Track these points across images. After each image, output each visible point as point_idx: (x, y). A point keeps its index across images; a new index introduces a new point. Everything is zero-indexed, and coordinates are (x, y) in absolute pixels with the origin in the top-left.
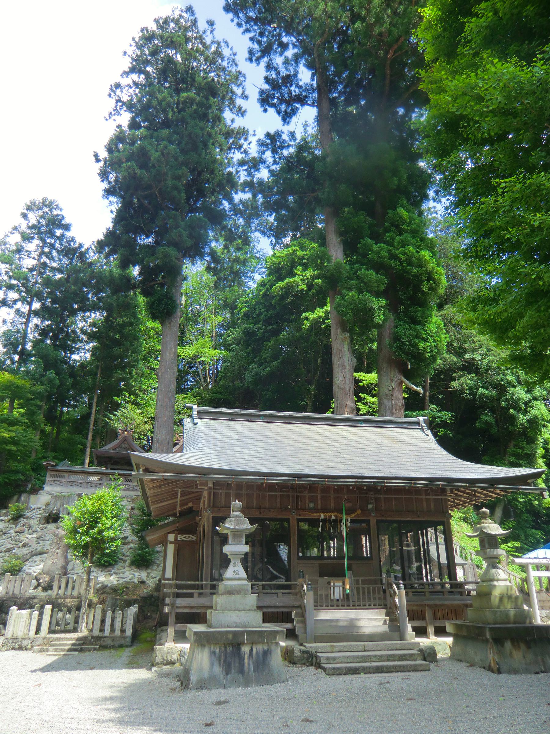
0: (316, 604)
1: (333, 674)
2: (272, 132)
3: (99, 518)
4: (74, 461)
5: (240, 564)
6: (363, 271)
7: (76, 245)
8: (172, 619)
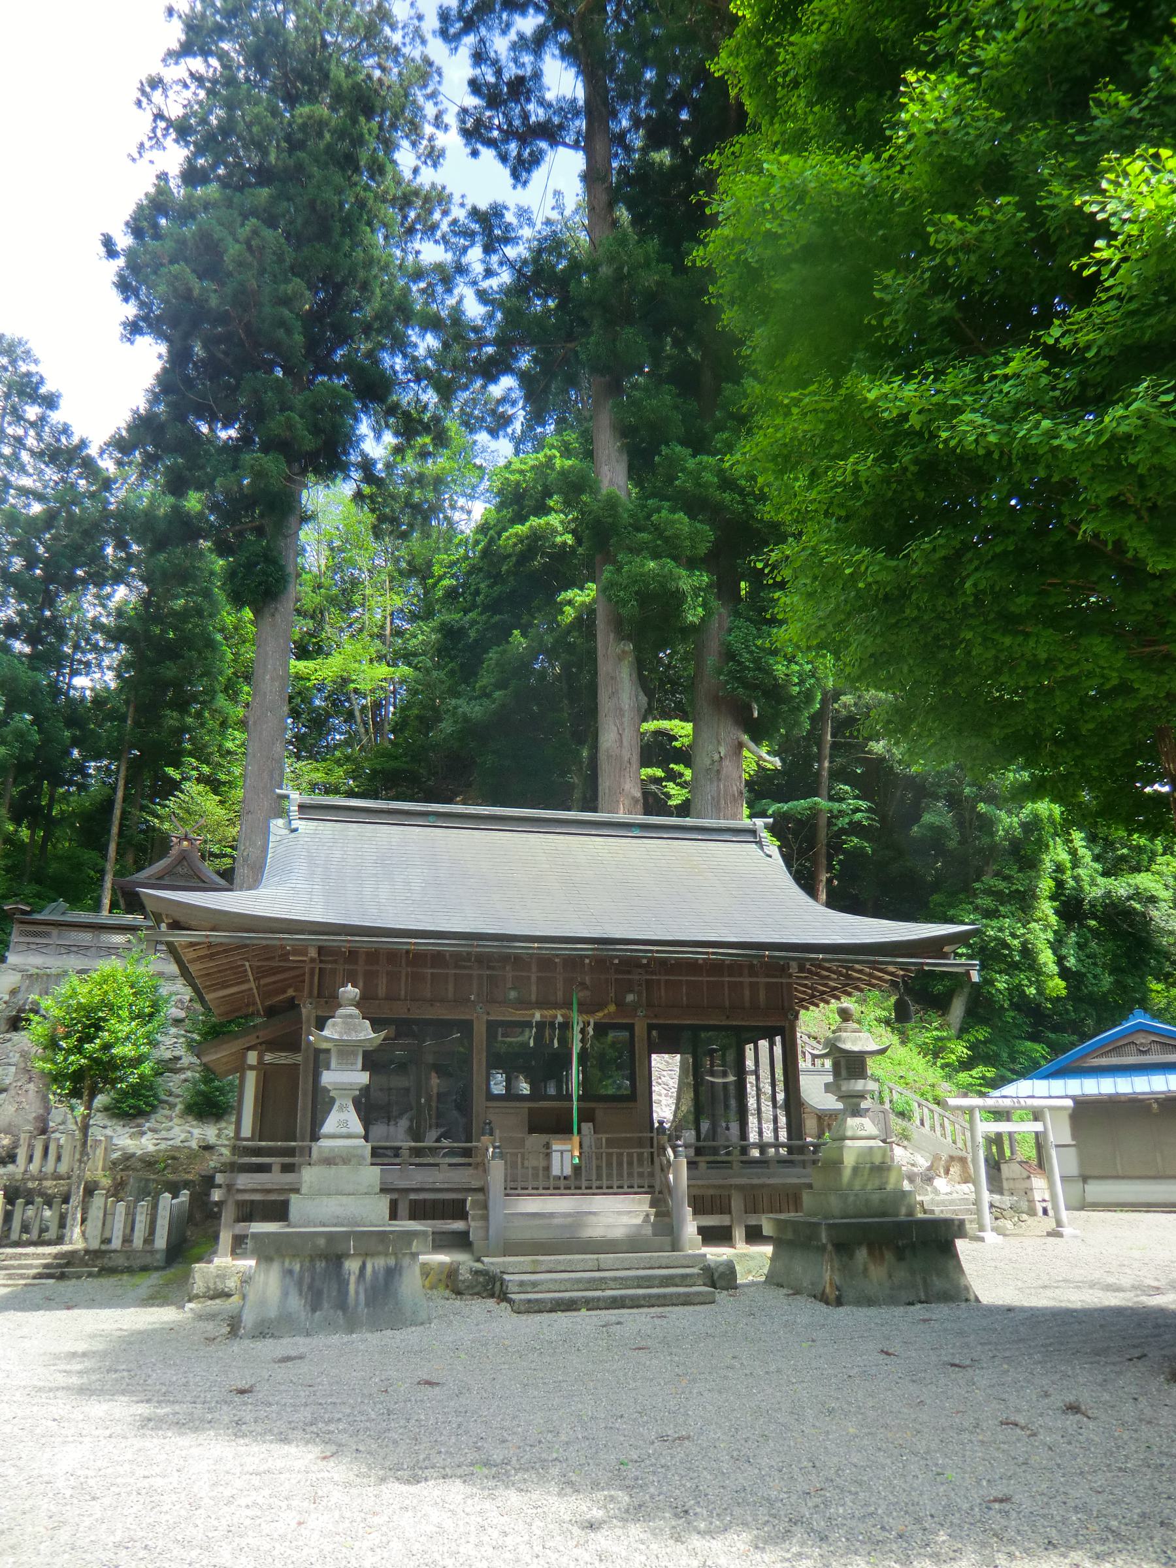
0: (512, 1185)
1: (528, 1312)
2: (483, 206)
3: (104, 1020)
4: (75, 901)
5: (351, 1108)
6: (664, 513)
7: (75, 440)
8: (228, 1214)
